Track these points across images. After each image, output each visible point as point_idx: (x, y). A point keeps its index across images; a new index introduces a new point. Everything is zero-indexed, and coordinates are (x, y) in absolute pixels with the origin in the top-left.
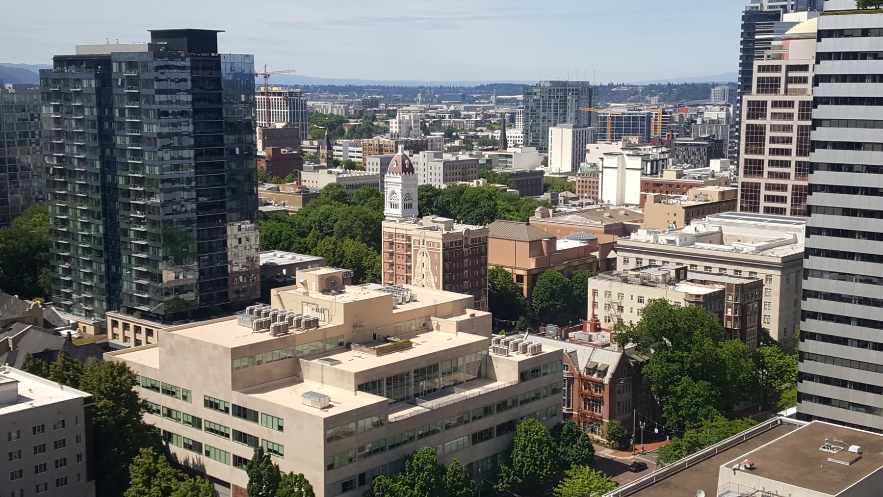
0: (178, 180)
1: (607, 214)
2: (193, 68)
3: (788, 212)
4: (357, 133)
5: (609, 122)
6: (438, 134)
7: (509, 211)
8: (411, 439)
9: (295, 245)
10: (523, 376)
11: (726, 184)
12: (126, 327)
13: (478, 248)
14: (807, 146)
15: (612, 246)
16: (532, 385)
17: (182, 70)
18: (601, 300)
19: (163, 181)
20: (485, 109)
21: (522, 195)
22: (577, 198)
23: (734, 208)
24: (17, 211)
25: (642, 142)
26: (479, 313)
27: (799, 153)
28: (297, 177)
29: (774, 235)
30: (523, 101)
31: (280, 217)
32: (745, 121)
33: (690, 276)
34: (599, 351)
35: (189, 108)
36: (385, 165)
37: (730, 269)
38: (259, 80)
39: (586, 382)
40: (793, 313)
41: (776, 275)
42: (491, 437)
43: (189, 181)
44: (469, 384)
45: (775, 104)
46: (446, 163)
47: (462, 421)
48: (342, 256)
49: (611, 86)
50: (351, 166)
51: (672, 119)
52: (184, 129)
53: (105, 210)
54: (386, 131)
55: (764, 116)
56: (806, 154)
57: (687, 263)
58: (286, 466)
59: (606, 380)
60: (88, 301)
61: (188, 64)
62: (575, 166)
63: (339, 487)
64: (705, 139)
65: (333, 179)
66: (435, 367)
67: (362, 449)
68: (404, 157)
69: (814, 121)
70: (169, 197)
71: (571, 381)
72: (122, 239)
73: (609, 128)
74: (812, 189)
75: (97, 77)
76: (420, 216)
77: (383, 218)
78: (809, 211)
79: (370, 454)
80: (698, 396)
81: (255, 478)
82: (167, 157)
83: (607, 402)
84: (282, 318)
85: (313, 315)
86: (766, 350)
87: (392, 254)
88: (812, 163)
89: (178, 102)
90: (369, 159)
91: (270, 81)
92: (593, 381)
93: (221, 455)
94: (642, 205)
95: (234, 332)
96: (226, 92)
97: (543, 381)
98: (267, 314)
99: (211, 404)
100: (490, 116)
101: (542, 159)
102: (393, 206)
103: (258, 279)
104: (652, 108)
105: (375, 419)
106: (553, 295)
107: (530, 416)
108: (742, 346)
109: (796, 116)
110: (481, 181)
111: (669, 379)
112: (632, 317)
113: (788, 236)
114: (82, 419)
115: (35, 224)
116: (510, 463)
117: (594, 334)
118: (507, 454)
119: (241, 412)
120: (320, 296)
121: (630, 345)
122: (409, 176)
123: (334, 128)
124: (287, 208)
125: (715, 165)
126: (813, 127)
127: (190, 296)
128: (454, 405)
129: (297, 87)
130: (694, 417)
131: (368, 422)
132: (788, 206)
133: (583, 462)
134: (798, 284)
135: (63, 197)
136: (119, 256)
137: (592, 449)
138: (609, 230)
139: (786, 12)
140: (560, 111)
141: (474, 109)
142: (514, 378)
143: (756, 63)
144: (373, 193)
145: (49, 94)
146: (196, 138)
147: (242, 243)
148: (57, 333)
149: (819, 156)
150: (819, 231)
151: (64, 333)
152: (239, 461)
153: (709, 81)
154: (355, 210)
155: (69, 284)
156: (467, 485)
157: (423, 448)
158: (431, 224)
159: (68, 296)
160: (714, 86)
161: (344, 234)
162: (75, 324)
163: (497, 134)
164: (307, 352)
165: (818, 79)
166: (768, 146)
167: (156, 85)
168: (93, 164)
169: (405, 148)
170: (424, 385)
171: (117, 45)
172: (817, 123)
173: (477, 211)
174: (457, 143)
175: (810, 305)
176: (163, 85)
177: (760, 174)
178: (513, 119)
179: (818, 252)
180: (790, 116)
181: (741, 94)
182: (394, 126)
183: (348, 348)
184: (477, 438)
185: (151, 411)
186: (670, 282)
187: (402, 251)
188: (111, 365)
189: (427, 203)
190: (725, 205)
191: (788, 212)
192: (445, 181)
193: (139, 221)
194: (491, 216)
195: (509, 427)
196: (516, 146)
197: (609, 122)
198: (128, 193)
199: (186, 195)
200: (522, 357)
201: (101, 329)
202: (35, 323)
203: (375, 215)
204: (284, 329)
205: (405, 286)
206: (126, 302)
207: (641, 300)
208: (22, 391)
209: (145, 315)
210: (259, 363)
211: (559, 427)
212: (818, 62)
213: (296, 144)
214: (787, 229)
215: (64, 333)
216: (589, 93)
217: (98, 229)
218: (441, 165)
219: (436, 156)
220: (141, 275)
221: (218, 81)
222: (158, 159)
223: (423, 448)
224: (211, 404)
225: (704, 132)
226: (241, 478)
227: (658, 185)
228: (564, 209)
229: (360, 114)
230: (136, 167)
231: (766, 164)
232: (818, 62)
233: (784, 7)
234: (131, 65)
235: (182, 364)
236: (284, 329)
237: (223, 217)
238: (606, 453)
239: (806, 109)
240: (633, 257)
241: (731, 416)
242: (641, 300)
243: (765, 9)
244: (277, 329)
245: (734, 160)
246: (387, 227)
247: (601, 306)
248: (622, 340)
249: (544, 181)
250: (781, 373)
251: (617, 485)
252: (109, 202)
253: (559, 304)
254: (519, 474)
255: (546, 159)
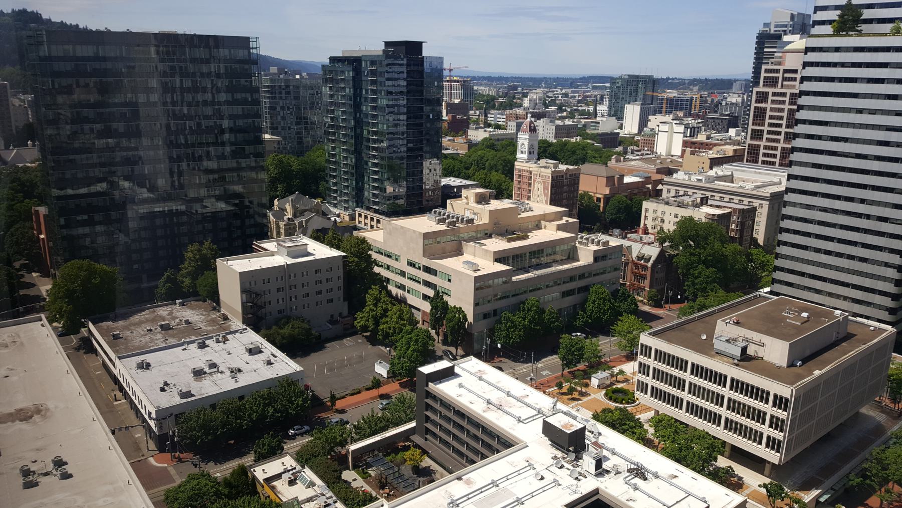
0: (397, 133)
1: (658, 161)
2: (408, 65)
3: (777, 164)
4: (503, 107)
5: (665, 102)
6: (554, 108)
7: (595, 157)
8: (525, 292)
9: (462, 174)
10: (596, 259)
11: (738, 145)
12: (366, 217)
13: (573, 179)
14: (793, 122)
15: (660, 182)
16: (601, 264)
17: (401, 67)
18: (650, 215)
19: (388, 134)
20: (584, 92)
21: (604, 147)
22: (640, 151)
23: (742, 161)
24: (308, 148)
25: (685, 116)
26: (571, 220)
27: (788, 127)
28: (465, 133)
29: (767, 179)
30: (610, 88)
31: (454, 157)
32: (754, 105)
33: (710, 202)
34: (646, 246)
35: (405, 90)
36: (519, 127)
37: (736, 199)
38: (446, 73)
39: (636, 265)
40: (774, 228)
41: (766, 204)
42: (573, 294)
43: (403, 134)
44: (562, 262)
45: (774, 94)
46: (557, 127)
47: (556, 284)
48: (490, 182)
49: (668, 79)
50: (498, 127)
51: (706, 102)
52: (401, 102)
53: (356, 149)
54: (521, 105)
55: (766, 102)
56: (792, 128)
57: (708, 194)
58: (452, 302)
59: (649, 265)
60: (346, 201)
61: (405, 62)
62: (641, 129)
63: (482, 316)
64: (727, 115)
65: (487, 135)
66: (542, 251)
67: (496, 296)
68: (531, 122)
69: (799, 106)
70: (392, 143)
71: (626, 264)
72: (365, 166)
73: (664, 106)
74: (793, 150)
75: (354, 70)
76: (539, 159)
77: (515, 159)
78: (791, 164)
79: (500, 299)
80: (708, 277)
81: (434, 307)
82: (391, 119)
83: (649, 278)
84: (453, 217)
85: (471, 216)
86: (755, 251)
87: (520, 182)
88: (795, 134)
89: (398, 86)
90: (509, 123)
91: (453, 73)
92: (641, 265)
93: (416, 293)
94: (682, 156)
95: (425, 223)
96: (426, 80)
97: (608, 263)
98: (444, 214)
99: (411, 264)
100: (588, 97)
101: (619, 125)
102: (523, 152)
103: (440, 193)
104: (693, 94)
105: (504, 279)
106: (619, 211)
107: (599, 283)
108: (739, 247)
109: (787, 103)
110: (578, 138)
111: (689, 266)
112: (670, 227)
113: (774, 179)
114: (341, 268)
115: (318, 156)
116: (584, 311)
117: (644, 236)
118: (582, 305)
119: (428, 270)
120: (475, 205)
121: (667, 244)
122: (533, 134)
123: (489, 103)
124: (459, 151)
125: (732, 132)
126: (798, 110)
127: (401, 202)
128: (552, 274)
129: (468, 77)
130: (704, 290)
131: (500, 280)
132: (777, 160)
133: (631, 313)
134: (779, 210)
135: (333, 141)
136: (363, 176)
137: (636, 305)
138: (659, 171)
139: (785, 34)
140: (634, 94)
141: (577, 92)
142: (590, 260)
143: (764, 67)
144: (511, 144)
145: (326, 79)
146: (408, 108)
147: (432, 172)
148: (329, 219)
149: (800, 129)
150: (796, 177)
151: (333, 219)
152: (425, 297)
153: (732, 78)
154: (499, 154)
155: (336, 191)
156: (557, 321)
157: (532, 298)
158: (545, 165)
159: (335, 198)
160: (735, 81)
161: (491, 168)
162: (339, 214)
163: (591, 108)
164: (466, 238)
165: (803, 79)
166: (767, 121)
167: (387, 75)
168: (350, 122)
169: (532, 117)
170: (534, 261)
171: (366, 50)
172: (800, 108)
173: (575, 157)
174: (565, 114)
175: (785, 224)
176: (390, 76)
177: (761, 139)
178: (602, 99)
179: (794, 191)
180: (783, 102)
181: (752, 87)
182: (526, 102)
183: (490, 237)
184: (565, 294)
185: (379, 266)
186: (697, 206)
187: (526, 180)
188: (357, 238)
189: (543, 151)
190: (736, 158)
191: (777, 164)
192: (556, 138)
193: (374, 157)
194: (583, 161)
195: (586, 289)
196: (603, 116)
197: (665, 102)
198: (368, 140)
199: (401, 142)
200: (597, 248)
201: (352, 218)
202: (317, 212)
203: (511, 158)
204: (454, 224)
205: (527, 202)
206: (366, 203)
207: (676, 216)
208: (310, 250)
209: (376, 211)
210: (439, 242)
211: (617, 291)
212: (804, 68)
213: (466, 113)
214: (776, 175)
215: (333, 219)
216: (653, 83)
217: (352, 161)
218: (554, 128)
219: (551, 122)
220: (375, 188)
221: (421, 73)
222: (386, 122)
223: (532, 298)
224: (411, 264)
225: (726, 110)
226: (426, 307)
227: (694, 143)
228: (631, 157)
229: (505, 95)
230: (374, 125)
231: (765, 132)
232: (804, 68)
233: (785, 31)
234: (373, 63)
235: (396, 240)
236: (454, 224)
237: (421, 156)
238: (646, 308)
239: (794, 98)
240: (673, 189)
241: (728, 290)
242: (676, 216)
243: (772, 32)
244: (450, 224)
245: (745, 129)
246: (518, 165)
247: (650, 219)
248: (662, 241)
249: (619, 139)
250: (763, 266)
251: (651, 328)
252: (359, 145)
253: (622, 217)
254: (590, 317)
255: (622, 125)
